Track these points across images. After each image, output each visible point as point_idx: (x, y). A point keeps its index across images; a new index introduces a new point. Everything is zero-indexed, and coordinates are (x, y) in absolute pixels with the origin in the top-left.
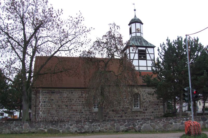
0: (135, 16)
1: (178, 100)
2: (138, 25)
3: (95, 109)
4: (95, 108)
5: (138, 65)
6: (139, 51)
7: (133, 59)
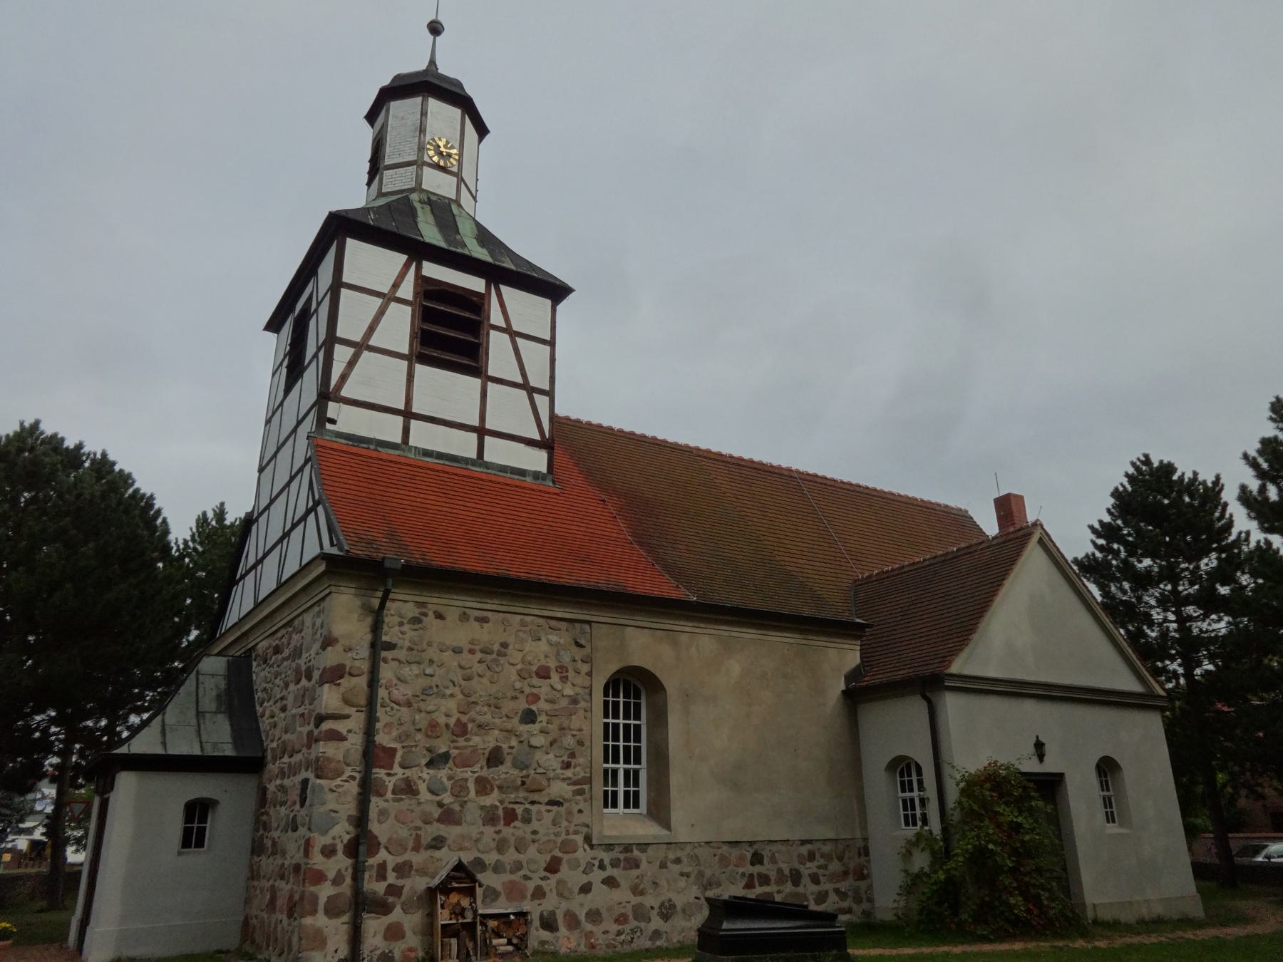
1: (1207, 650)
2: (443, 116)
3: (610, 810)
4: (615, 805)
6: (430, 291)
7: (361, 347)
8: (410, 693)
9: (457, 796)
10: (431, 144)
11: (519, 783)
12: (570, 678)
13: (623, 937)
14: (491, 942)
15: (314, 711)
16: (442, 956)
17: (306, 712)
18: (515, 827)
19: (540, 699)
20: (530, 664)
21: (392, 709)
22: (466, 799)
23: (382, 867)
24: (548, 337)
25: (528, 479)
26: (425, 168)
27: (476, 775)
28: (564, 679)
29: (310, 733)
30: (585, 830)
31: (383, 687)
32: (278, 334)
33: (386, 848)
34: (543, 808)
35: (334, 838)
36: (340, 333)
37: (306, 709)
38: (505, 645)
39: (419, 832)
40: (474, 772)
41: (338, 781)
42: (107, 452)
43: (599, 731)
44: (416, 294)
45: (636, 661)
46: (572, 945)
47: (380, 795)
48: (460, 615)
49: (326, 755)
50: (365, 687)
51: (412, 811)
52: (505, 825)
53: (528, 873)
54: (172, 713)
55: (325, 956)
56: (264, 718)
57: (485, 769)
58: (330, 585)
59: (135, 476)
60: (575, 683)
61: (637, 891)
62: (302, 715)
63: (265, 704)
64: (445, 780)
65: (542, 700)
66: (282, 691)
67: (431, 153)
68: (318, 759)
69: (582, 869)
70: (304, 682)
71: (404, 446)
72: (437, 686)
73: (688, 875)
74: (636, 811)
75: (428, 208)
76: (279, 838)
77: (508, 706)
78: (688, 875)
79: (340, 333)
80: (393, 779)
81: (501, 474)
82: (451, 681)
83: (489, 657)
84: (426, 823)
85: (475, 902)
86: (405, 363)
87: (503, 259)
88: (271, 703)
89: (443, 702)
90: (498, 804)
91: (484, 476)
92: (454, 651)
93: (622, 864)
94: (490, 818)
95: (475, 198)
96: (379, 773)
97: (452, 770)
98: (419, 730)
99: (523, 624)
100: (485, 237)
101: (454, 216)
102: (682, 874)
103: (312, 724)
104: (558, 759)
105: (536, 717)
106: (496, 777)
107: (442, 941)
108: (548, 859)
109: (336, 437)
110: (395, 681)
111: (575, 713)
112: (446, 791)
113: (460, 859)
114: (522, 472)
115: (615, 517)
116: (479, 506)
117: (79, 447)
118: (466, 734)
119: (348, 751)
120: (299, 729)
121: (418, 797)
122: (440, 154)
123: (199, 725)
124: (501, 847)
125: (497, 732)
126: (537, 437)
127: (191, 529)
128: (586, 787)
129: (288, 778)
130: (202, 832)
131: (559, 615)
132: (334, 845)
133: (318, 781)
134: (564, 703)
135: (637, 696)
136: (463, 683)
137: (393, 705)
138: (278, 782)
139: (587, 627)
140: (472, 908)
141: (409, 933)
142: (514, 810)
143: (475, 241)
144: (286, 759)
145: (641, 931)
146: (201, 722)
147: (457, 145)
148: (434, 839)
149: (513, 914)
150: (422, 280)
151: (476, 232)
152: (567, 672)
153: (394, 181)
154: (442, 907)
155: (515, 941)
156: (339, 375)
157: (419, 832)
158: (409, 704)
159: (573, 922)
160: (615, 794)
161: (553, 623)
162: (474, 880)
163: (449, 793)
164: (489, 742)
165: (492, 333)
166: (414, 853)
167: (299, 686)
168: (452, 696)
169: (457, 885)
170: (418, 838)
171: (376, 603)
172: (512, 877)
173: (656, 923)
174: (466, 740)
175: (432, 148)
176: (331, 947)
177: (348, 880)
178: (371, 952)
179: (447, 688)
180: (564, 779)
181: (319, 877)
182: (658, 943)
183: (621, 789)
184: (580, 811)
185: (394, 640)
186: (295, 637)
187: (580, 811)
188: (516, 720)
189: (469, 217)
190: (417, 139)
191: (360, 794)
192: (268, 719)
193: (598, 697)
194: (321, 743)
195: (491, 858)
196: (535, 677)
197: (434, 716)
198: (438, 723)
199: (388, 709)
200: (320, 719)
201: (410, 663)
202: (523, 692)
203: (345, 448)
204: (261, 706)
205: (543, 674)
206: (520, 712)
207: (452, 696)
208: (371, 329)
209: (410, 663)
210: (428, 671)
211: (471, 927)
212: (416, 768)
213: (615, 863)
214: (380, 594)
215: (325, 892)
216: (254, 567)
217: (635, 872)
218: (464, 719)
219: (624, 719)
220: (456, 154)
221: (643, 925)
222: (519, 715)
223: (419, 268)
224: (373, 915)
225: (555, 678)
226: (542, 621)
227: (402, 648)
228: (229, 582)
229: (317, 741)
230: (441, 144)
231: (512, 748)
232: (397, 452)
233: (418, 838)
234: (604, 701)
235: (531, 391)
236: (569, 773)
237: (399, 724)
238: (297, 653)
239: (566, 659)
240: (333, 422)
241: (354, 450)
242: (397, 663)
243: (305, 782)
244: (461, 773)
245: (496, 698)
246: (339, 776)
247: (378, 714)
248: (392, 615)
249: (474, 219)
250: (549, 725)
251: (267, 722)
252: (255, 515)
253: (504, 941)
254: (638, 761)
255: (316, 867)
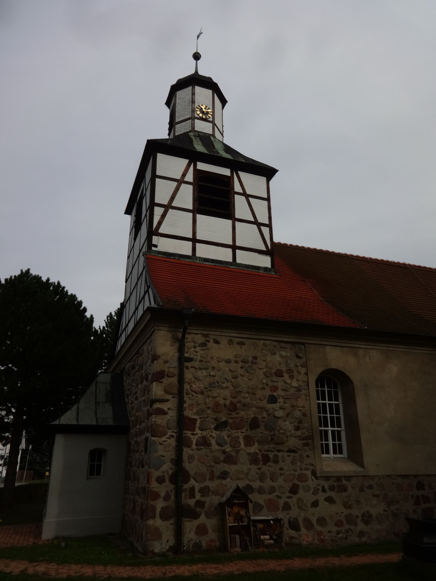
0: (198, 39)
4: (328, 452)
5: (191, 236)
6: (198, 173)
7: (168, 207)
8: (202, 386)
9: (233, 447)
10: (198, 108)
11: (270, 438)
12: (295, 376)
13: (341, 535)
14: (260, 538)
15: (149, 398)
16: (231, 546)
17: (146, 399)
18: (269, 466)
19: (278, 388)
20: (271, 368)
21: (193, 395)
22: (239, 449)
23: (192, 489)
24: (265, 196)
25: (261, 271)
26: (196, 120)
27: (244, 434)
28: (291, 377)
29: (148, 410)
30: (312, 467)
31: (187, 383)
32: (131, 215)
33: (194, 478)
34: (285, 454)
35: (163, 472)
36: (157, 201)
37: (145, 397)
38: (255, 358)
39: (212, 469)
40: (242, 433)
41: (164, 438)
42: (60, 282)
43: (315, 409)
44: (194, 178)
45: (334, 366)
46: (310, 539)
47: (189, 446)
48: (228, 341)
49: (157, 423)
50: (177, 383)
51: (208, 456)
52: (263, 464)
53: (279, 494)
54: (82, 404)
55: (161, 544)
56: (129, 405)
57: (249, 431)
58: (154, 326)
59: (77, 296)
60: (298, 379)
61: (347, 505)
62: (144, 401)
63: (129, 397)
64: (226, 437)
65: (280, 390)
66: (136, 389)
67: (198, 112)
68: (152, 425)
69: (312, 491)
70: (145, 382)
71: (193, 257)
72: (218, 382)
73: (377, 496)
74: (341, 456)
75: (198, 138)
76: (136, 471)
77: (260, 393)
78: (377, 496)
79: (157, 201)
80: (196, 437)
81: (246, 269)
82: (225, 379)
83: (247, 365)
84: (216, 463)
85: (248, 512)
86: (191, 214)
87: (239, 158)
88: (131, 396)
89: (222, 391)
90: (258, 452)
91: (237, 270)
92: (226, 362)
93: (336, 489)
94: (254, 459)
95: (222, 135)
96: (187, 434)
97: (229, 431)
98: (209, 408)
99: (265, 345)
100: (228, 149)
101: (212, 141)
102: (374, 496)
103: (149, 405)
104: (292, 424)
105: (277, 400)
106: (256, 436)
107: (230, 537)
108: (291, 485)
109: (158, 254)
110: (193, 380)
111: (300, 397)
112: (227, 444)
113: (238, 485)
114: (258, 268)
115: (311, 289)
116: (235, 285)
117: (48, 280)
118: (237, 410)
119: (169, 420)
120: (143, 409)
121: (210, 448)
122: (203, 112)
123: (96, 409)
124: (262, 478)
125: (254, 409)
126: (264, 249)
127: (105, 321)
128: (310, 441)
129: (139, 437)
130: (99, 467)
131: (286, 340)
132: (164, 477)
133: (153, 438)
134: (292, 391)
135: (335, 387)
136: (233, 380)
137: (193, 393)
138: (135, 439)
139: (302, 347)
140: (247, 515)
141: (210, 531)
142: (268, 455)
143: (223, 152)
144: (138, 426)
145: (352, 531)
146: (98, 407)
147: (211, 107)
148: (222, 473)
149: (272, 520)
150: (197, 172)
151: (224, 148)
152: (293, 372)
153: (180, 129)
154: (229, 515)
155: (274, 537)
156: (157, 222)
157: (212, 469)
158: (202, 393)
159: (309, 525)
160: (327, 445)
161: (283, 344)
162: (247, 499)
163: (228, 445)
164: (250, 415)
165: (236, 196)
166: (210, 481)
167: (143, 385)
168: (227, 387)
169: (237, 502)
170: (212, 473)
171: (180, 335)
172: (270, 496)
173: (361, 526)
174: (236, 414)
175: (199, 110)
176: (165, 537)
177: (173, 498)
178: (188, 542)
179: (224, 383)
180: (296, 437)
181: (156, 496)
182: (364, 539)
183: (331, 442)
184: (308, 456)
185: (192, 356)
186: (140, 359)
187: (308, 456)
188: (265, 402)
189: (220, 142)
190: (191, 107)
191: (176, 446)
192: (130, 405)
193: (313, 388)
194: (154, 416)
195: (256, 484)
196: (274, 376)
197: (217, 399)
198: (219, 404)
199: (190, 396)
200: (153, 402)
201: (201, 369)
202: (268, 385)
203: (162, 259)
204: (127, 398)
205: (279, 374)
206: (267, 397)
207: (227, 387)
208: (173, 198)
209: (201, 369)
210: (212, 374)
211: (247, 527)
212: (209, 430)
213: (332, 488)
214: (181, 330)
215: (160, 505)
216: (125, 329)
217: (344, 494)
218: (235, 401)
219: (328, 401)
220: (211, 112)
221: (352, 527)
222: (267, 398)
223: (195, 166)
224: (189, 519)
225: (286, 376)
226: (275, 343)
227: (196, 360)
228: (117, 338)
229: (151, 415)
230: (203, 107)
231: (264, 418)
232: (189, 260)
233: (212, 473)
234: (317, 390)
235: (259, 225)
236: (299, 433)
237: (197, 405)
238: (141, 367)
239: (292, 365)
240: (156, 246)
241: (168, 260)
242: (194, 369)
243: (147, 439)
244: (235, 433)
245: (253, 388)
246: (164, 435)
247: (185, 399)
248: (189, 342)
249: (223, 142)
250: (285, 404)
251: (130, 406)
252: (125, 303)
253: (267, 537)
254: (339, 426)
255: (154, 489)
